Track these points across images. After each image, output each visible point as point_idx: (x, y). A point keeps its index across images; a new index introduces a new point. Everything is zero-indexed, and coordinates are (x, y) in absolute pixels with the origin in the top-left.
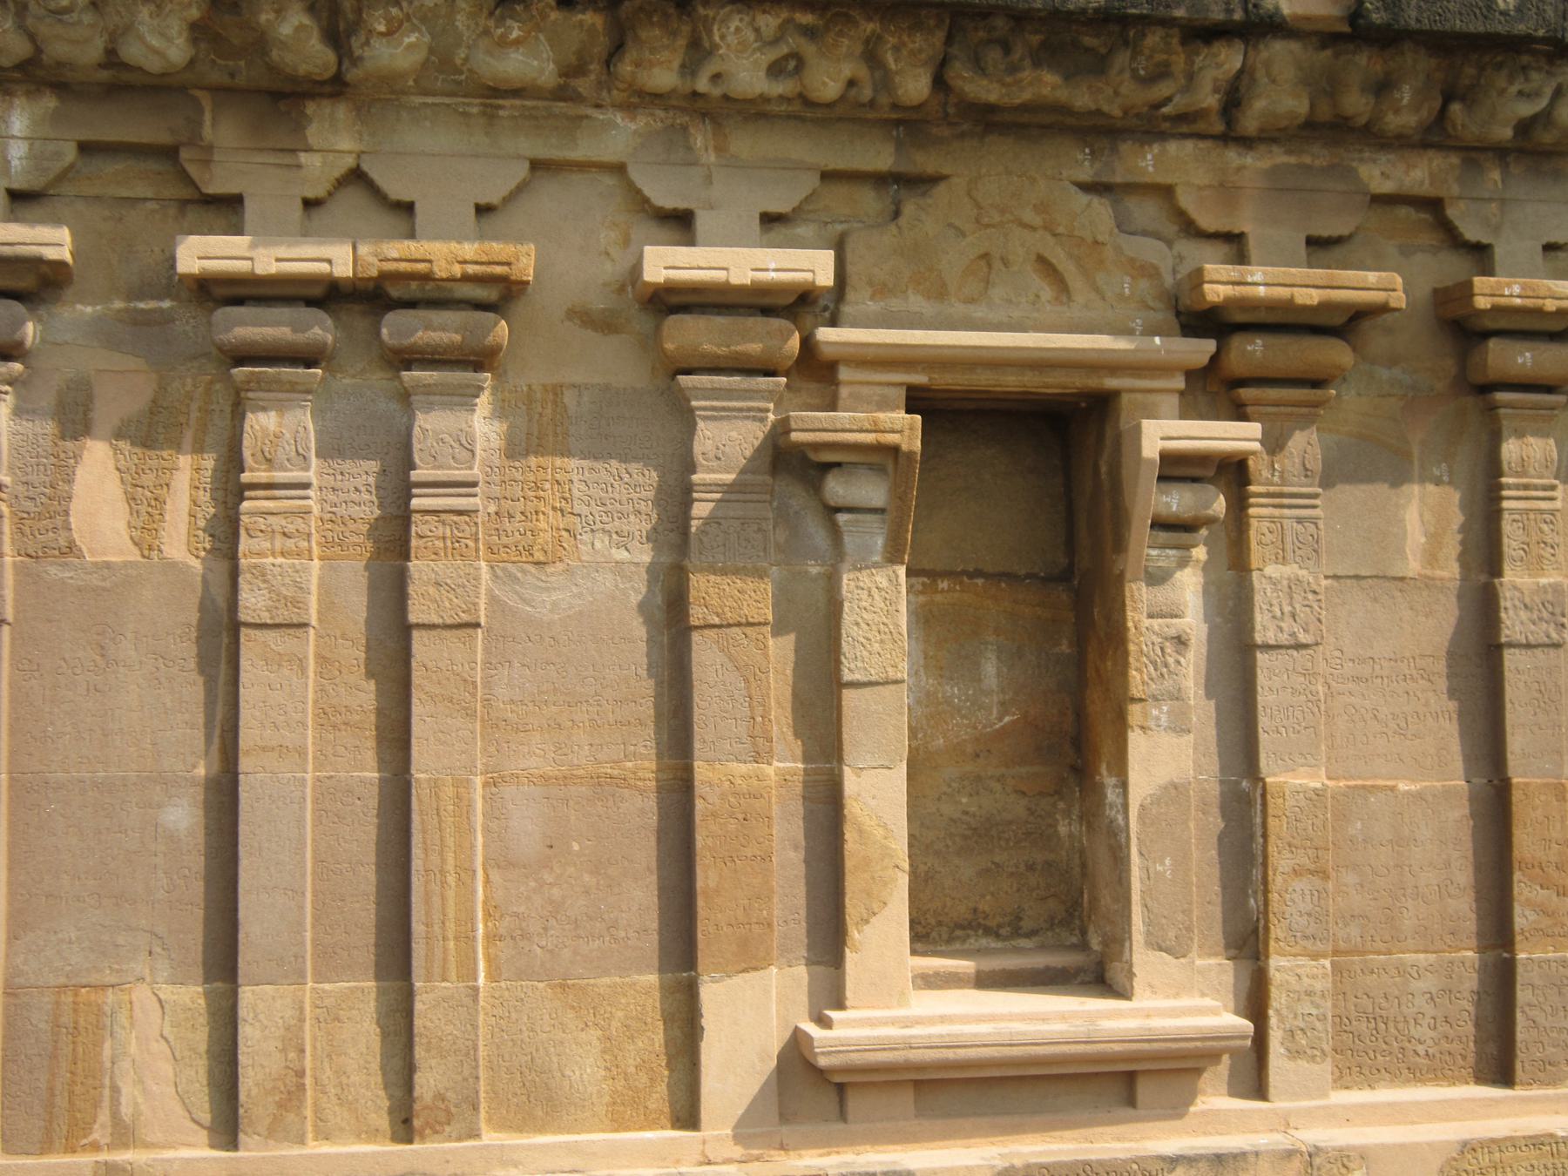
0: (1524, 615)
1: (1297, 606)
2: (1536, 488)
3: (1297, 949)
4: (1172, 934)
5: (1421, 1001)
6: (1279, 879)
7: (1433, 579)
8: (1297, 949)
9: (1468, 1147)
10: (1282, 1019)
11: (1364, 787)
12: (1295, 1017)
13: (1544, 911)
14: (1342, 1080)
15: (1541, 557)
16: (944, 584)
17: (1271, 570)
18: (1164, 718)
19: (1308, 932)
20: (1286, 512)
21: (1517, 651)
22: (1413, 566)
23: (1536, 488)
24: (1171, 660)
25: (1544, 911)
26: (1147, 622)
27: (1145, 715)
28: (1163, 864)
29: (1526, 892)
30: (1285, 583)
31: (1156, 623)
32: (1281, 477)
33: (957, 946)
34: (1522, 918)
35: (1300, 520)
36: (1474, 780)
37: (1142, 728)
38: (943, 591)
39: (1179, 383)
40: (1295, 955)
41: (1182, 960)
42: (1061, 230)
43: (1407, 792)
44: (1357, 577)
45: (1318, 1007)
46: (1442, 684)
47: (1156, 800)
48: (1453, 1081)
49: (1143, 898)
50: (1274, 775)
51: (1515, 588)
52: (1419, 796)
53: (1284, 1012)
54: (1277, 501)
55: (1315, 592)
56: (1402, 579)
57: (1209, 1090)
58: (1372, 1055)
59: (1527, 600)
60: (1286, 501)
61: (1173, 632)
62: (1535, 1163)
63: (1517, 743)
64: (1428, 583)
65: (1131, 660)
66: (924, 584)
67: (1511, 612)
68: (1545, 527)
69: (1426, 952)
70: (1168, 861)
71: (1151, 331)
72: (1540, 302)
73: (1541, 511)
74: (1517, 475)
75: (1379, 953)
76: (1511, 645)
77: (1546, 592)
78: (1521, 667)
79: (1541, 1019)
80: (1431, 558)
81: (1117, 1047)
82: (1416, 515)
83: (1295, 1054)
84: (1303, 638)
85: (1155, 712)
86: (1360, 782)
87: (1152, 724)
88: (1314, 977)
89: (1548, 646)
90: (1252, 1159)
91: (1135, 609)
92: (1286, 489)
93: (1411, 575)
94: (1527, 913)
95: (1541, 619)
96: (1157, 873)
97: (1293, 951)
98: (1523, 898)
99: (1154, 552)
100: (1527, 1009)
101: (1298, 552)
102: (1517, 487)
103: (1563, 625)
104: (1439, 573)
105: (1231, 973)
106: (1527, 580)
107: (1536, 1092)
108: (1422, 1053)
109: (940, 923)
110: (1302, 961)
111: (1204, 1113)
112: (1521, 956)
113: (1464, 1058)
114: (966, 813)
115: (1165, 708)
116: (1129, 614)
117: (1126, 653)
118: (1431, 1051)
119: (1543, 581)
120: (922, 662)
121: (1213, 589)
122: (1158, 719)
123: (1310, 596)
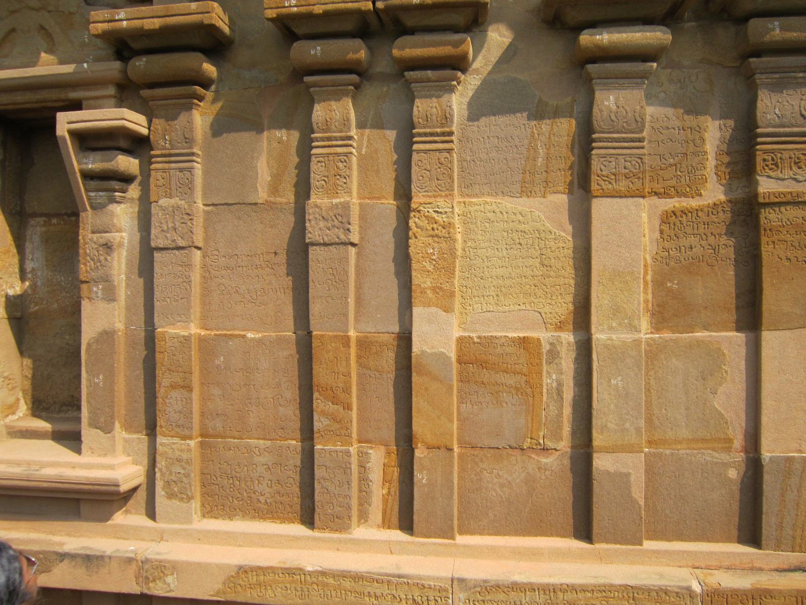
0: (322, 224)
1: (177, 224)
2: (336, 139)
3: (173, 433)
4: (102, 419)
5: (261, 469)
6: (162, 390)
7: (275, 204)
8: (173, 433)
9: (243, 570)
10: (163, 474)
11: (225, 335)
12: (171, 473)
13: (334, 419)
14: (209, 512)
15: (336, 185)
16: (54, 221)
17: (163, 202)
18: (100, 293)
19: (180, 423)
20: (173, 165)
21: (318, 248)
22: (262, 195)
23: (336, 139)
24: (102, 258)
25: (334, 419)
26: (90, 236)
27: (90, 291)
28: (98, 378)
29: (321, 405)
30: (171, 209)
31: (95, 236)
32: (170, 144)
33: (62, 415)
34: (319, 423)
35: (181, 170)
36: (298, 332)
37: (89, 298)
38: (54, 225)
39: (111, 91)
40: (172, 437)
41: (108, 435)
42: (51, 8)
43: (253, 339)
44: (226, 204)
45: (184, 469)
46: (283, 269)
47: (97, 341)
48: (283, 520)
49: (87, 398)
50: (163, 327)
51: (317, 206)
52: (260, 342)
53: (164, 470)
54: (167, 159)
55: (188, 214)
56: (256, 204)
57: (133, 511)
58: (231, 499)
59: (324, 214)
60: (173, 159)
61: (102, 241)
62: (288, 586)
63: (315, 308)
64: (270, 206)
65: (81, 258)
66: (45, 221)
67: (313, 222)
68: (340, 165)
69: (264, 439)
70: (101, 377)
71: (98, 60)
72: (312, 7)
73: (338, 154)
74: (324, 131)
75: (235, 438)
76: (313, 244)
77: (337, 208)
78: (320, 258)
79: (331, 488)
80: (274, 189)
81: (45, 485)
82: (265, 163)
83: (171, 496)
84: (181, 243)
85: (95, 289)
86: (225, 332)
87: (94, 296)
88: (182, 451)
89: (338, 244)
90: (107, 560)
91: (83, 229)
92: (172, 152)
93: (260, 201)
94: (322, 419)
95: (334, 226)
96: (95, 383)
97: (170, 434)
98: (319, 410)
99: (93, 194)
100: (322, 481)
101: (180, 190)
102: (323, 139)
103: (348, 230)
104: (279, 199)
105: (146, 444)
106: (326, 200)
107: (327, 535)
108: (263, 501)
109: (55, 403)
110: (176, 440)
111: (115, 526)
112: (318, 447)
113: (291, 507)
114: (68, 344)
115: (100, 287)
116: (81, 231)
117: (77, 254)
118: (268, 501)
119: (335, 201)
120: (45, 263)
121: (142, 215)
122: (97, 293)
123: (186, 217)
